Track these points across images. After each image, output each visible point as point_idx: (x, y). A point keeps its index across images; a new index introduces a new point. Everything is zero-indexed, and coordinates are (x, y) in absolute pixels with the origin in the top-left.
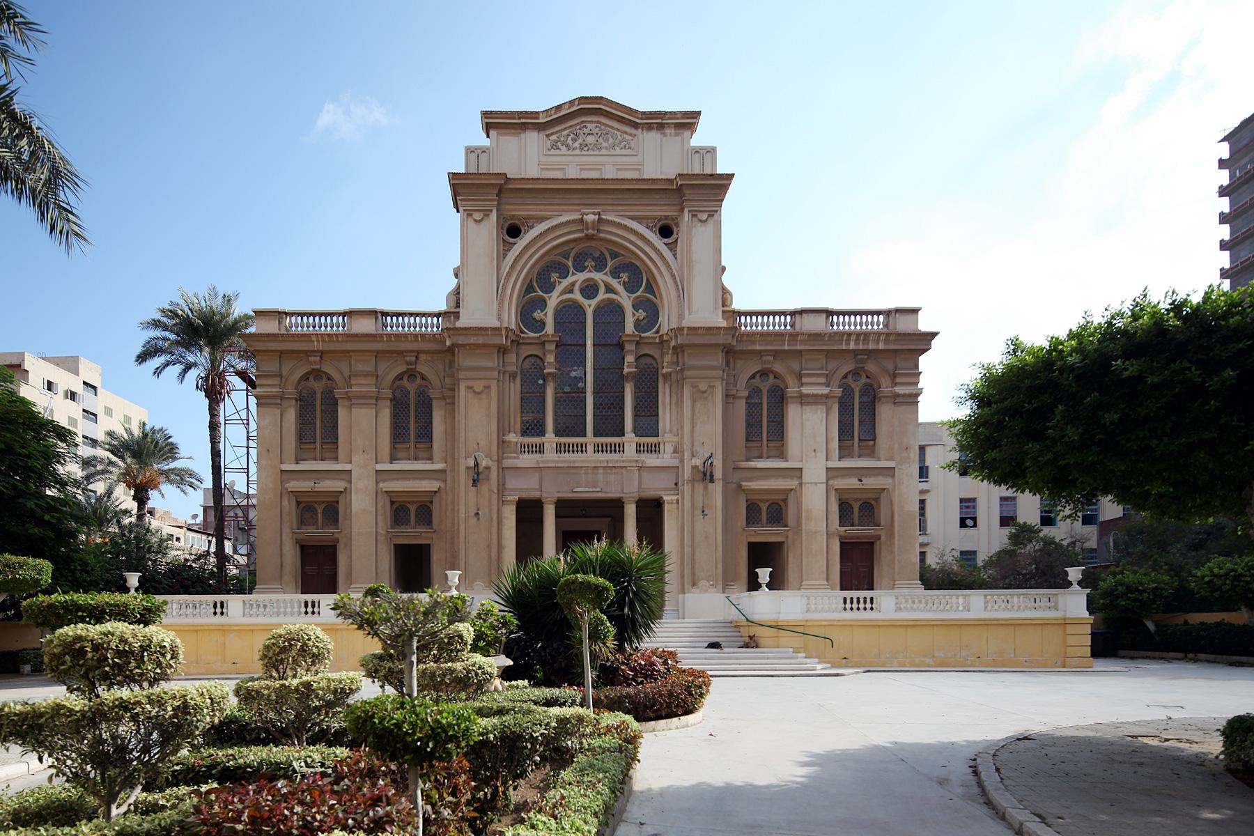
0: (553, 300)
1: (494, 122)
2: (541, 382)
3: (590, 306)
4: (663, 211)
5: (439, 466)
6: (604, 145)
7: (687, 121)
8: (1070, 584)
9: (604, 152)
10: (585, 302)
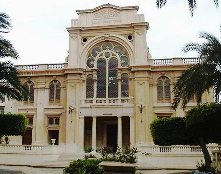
0: (97, 59)
1: (79, 12)
2: (122, 81)
3: (107, 60)
6: (111, 16)
7: (136, 8)
8: (52, 144)
10: (106, 59)
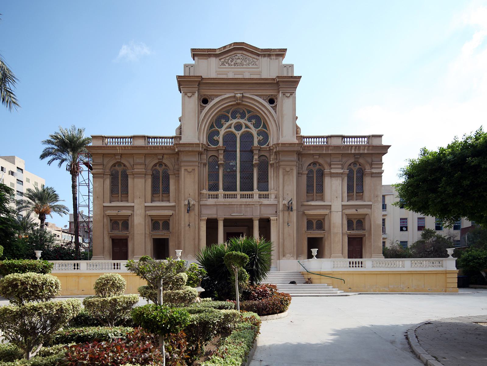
0: (222, 131)
1: (196, 53)
2: (217, 167)
3: (238, 134)
4: (270, 92)
5: (172, 204)
6: (245, 63)
7: (281, 53)
8: (448, 256)
9: (244, 66)
10: (236, 132)
